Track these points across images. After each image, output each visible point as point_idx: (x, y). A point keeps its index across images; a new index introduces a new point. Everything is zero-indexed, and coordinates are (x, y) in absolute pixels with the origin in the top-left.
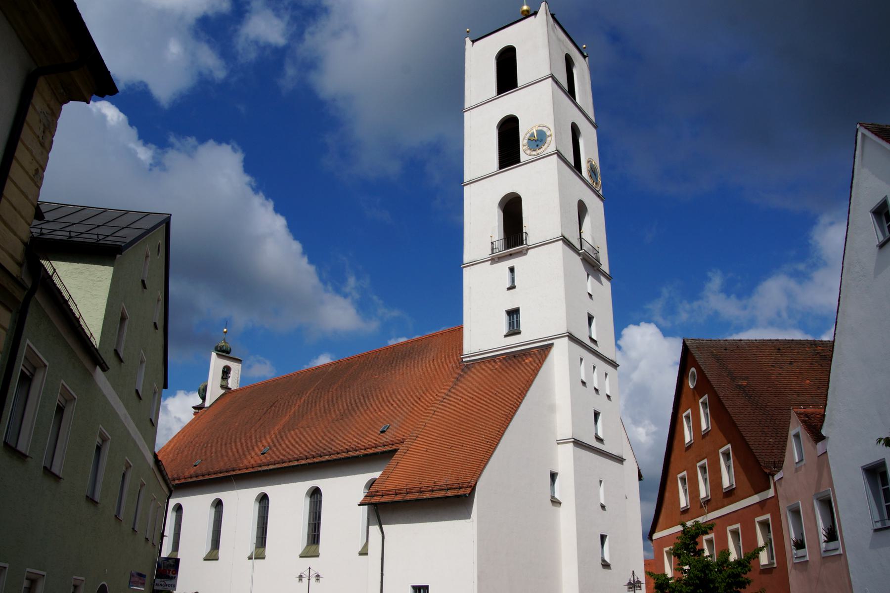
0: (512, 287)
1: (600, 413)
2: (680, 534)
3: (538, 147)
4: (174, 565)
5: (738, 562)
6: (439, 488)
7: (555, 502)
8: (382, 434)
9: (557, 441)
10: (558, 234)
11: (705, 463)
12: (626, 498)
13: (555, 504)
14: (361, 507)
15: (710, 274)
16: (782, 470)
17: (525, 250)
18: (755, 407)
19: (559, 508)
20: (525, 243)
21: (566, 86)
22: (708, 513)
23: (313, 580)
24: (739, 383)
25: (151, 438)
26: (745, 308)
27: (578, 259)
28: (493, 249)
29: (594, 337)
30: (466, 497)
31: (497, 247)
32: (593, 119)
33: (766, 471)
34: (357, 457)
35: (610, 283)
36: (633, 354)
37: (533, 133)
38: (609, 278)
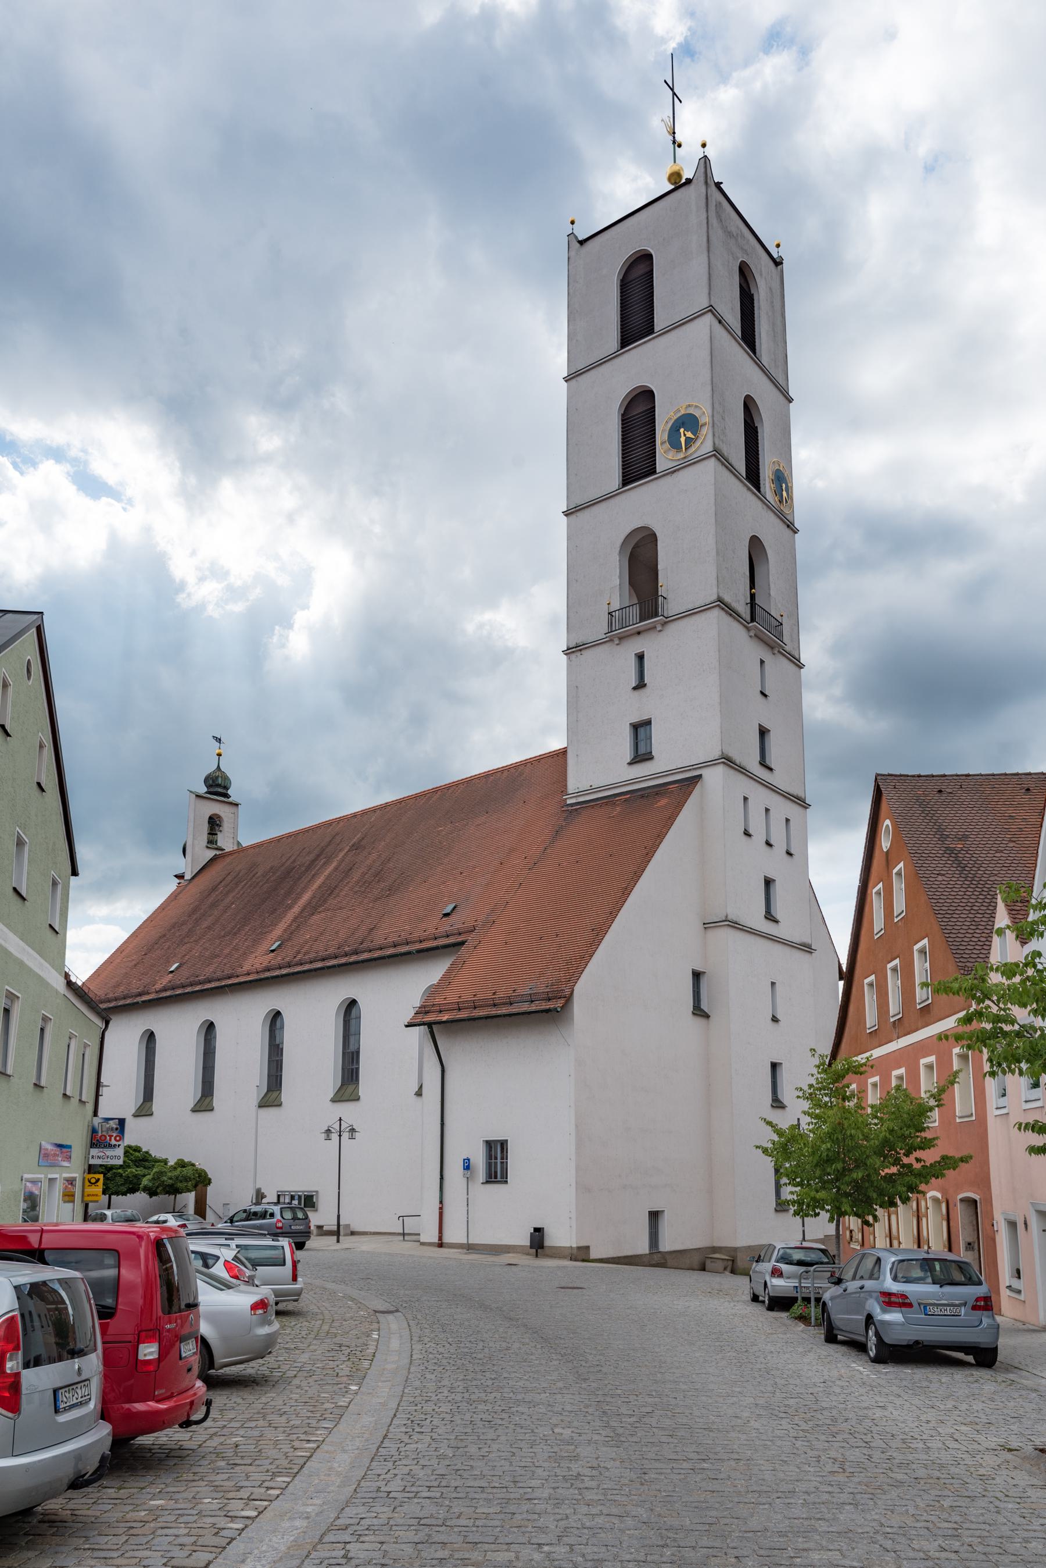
4: (117, 1129)
9: (704, 924)
23: (345, 1136)
25: (57, 956)
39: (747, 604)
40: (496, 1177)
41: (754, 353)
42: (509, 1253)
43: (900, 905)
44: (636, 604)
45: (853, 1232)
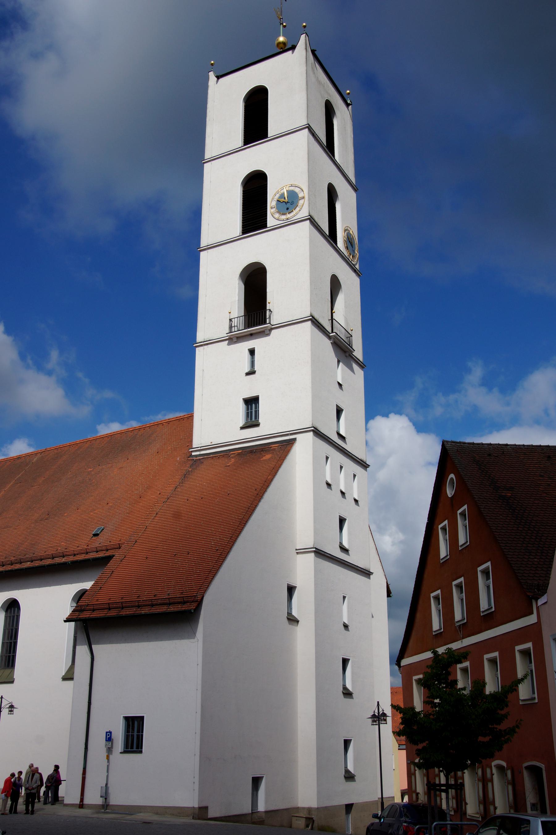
0: (252, 372)
1: (346, 519)
2: (430, 663)
3: (288, 210)
5: (493, 696)
6: (160, 602)
7: (292, 620)
8: (94, 538)
10: (306, 313)
11: (461, 582)
12: (373, 617)
13: (293, 623)
14: (68, 623)
15: (470, 364)
16: (546, 594)
17: (268, 331)
18: (519, 521)
19: (296, 627)
20: (268, 322)
21: (324, 139)
22: (463, 638)
24: (503, 494)
26: (508, 404)
27: (327, 343)
28: (231, 327)
29: (342, 432)
30: (192, 613)
31: (236, 325)
32: (353, 179)
33: (528, 594)
34: (65, 564)
35: (363, 372)
36: (381, 450)
37: (284, 193)
38: (362, 366)
39: (329, 320)
40: (132, 748)
42: (141, 813)
43: (462, 539)
44: (242, 316)
45: (419, 795)
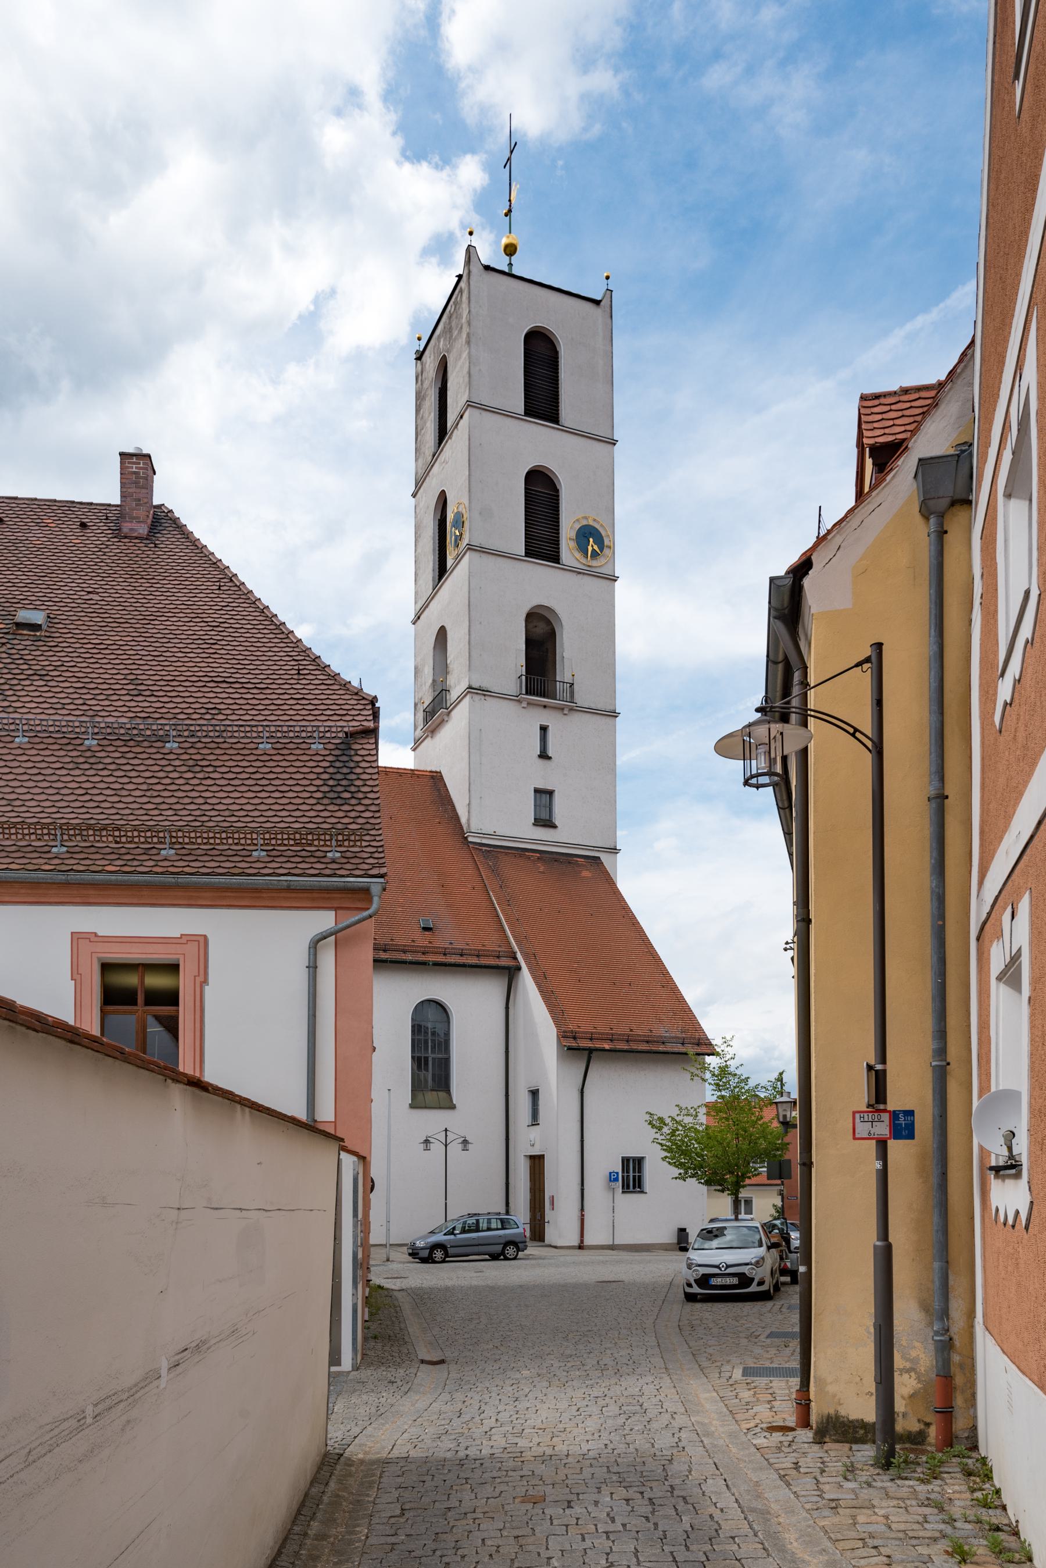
23: (455, 1148)
41: (440, 443)
